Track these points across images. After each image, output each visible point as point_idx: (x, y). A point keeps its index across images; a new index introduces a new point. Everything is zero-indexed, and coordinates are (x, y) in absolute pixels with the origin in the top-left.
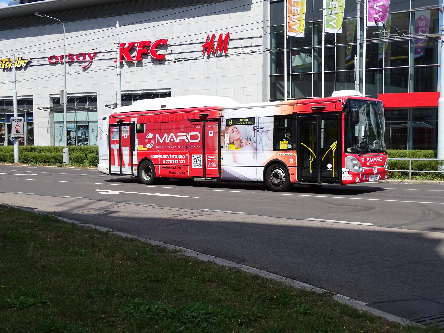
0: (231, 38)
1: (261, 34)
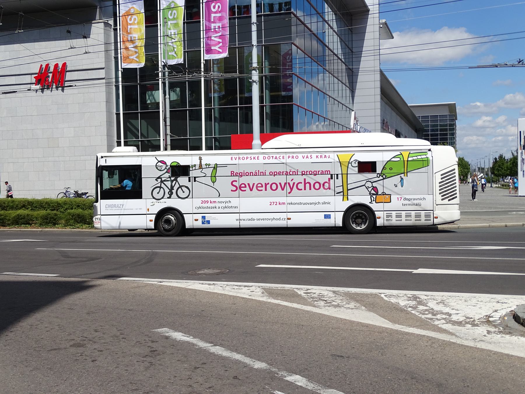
1: (103, 66)
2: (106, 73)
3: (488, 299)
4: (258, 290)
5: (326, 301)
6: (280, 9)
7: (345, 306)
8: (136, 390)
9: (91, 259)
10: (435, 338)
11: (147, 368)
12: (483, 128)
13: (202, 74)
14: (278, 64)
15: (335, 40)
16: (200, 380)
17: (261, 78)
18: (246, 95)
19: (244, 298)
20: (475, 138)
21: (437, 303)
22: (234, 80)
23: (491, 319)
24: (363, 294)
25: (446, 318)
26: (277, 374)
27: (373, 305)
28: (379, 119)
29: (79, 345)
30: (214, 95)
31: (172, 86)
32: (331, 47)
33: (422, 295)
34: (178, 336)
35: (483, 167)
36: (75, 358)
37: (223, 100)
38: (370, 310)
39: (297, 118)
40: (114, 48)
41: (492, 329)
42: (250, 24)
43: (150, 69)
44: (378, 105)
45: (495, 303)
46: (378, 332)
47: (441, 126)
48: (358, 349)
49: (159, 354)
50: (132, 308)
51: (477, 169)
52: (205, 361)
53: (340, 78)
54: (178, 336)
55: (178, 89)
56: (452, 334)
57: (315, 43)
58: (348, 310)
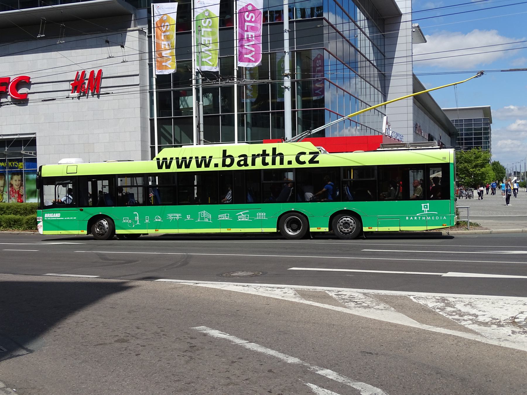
0: (103, 76)
1: (138, 73)
2: (141, 80)
3: (516, 301)
4: (291, 291)
5: (356, 302)
6: (312, 15)
7: (375, 307)
8: (178, 380)
9: (129, 261)
10: (461, 338)
11: (187, 362)
12: (518, 131)
13: (235, 80)
14: (309, 70)
15: (367, 45)
16: (237, 372)
17: (293, 84)
18: (278, 100)
19: (277, 299)
20: (509, 142)
21: (465, 305)
22: (267, 85)
23: (516, 320)
24: (392, 296)
25: (472, 319)
26: (309, 368)
27: (402, 307)
28: (411, 124)
29: (122, 341)
30: (247, 101)
31: (205, 92)
32: (363, 52)
33: (450, 297)
34: (216, 333)
35: (519, 171)
36: (120, 352)
37: (255, 105)
38: (399, 311)
40: (150, 55)
41: (517, 330)
42: (282, 32)
43: (183, 74)
44: (411, 109)
45: (521, 306)
46: (406, 332)
47: (475, 129)
48: (386, 347)
49: (198, 350)
50: (170, 307)
51: (513, 174)
52: (241, 356)
53: (372, 83)
54: (216, 333)
55: (211, 95)
56: (477, 334)
57: (346, 45)
58: (378, 311)
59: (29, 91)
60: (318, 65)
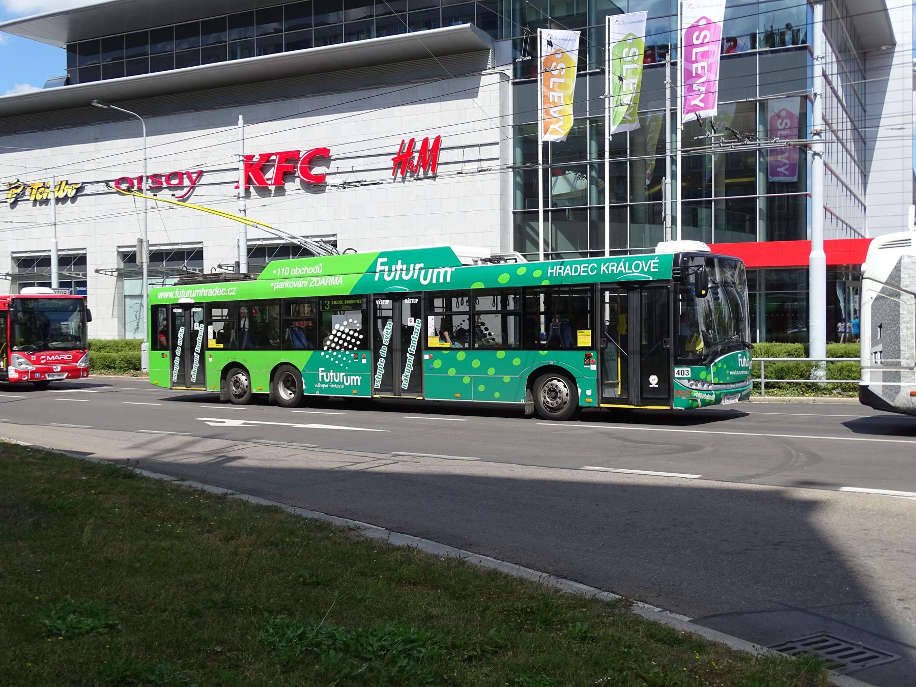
39: (685, 228)
59: (328, 171)
60: (780, 127)
